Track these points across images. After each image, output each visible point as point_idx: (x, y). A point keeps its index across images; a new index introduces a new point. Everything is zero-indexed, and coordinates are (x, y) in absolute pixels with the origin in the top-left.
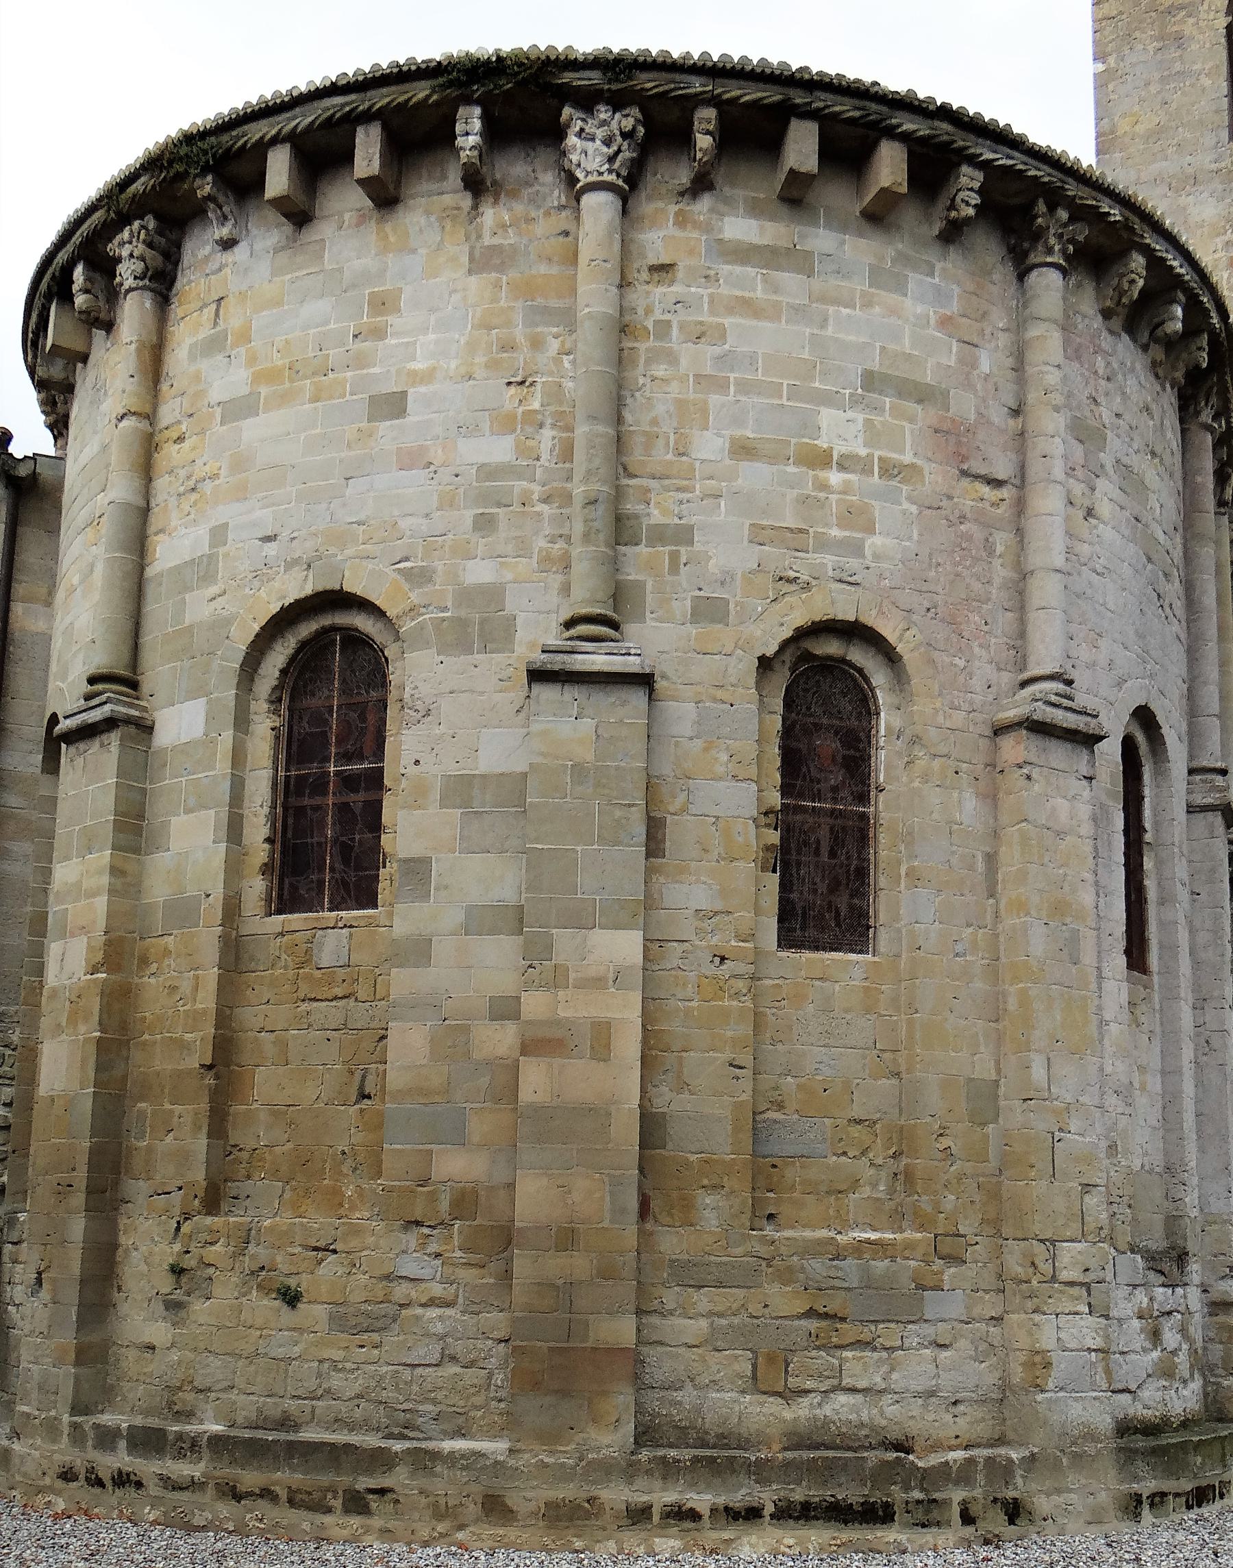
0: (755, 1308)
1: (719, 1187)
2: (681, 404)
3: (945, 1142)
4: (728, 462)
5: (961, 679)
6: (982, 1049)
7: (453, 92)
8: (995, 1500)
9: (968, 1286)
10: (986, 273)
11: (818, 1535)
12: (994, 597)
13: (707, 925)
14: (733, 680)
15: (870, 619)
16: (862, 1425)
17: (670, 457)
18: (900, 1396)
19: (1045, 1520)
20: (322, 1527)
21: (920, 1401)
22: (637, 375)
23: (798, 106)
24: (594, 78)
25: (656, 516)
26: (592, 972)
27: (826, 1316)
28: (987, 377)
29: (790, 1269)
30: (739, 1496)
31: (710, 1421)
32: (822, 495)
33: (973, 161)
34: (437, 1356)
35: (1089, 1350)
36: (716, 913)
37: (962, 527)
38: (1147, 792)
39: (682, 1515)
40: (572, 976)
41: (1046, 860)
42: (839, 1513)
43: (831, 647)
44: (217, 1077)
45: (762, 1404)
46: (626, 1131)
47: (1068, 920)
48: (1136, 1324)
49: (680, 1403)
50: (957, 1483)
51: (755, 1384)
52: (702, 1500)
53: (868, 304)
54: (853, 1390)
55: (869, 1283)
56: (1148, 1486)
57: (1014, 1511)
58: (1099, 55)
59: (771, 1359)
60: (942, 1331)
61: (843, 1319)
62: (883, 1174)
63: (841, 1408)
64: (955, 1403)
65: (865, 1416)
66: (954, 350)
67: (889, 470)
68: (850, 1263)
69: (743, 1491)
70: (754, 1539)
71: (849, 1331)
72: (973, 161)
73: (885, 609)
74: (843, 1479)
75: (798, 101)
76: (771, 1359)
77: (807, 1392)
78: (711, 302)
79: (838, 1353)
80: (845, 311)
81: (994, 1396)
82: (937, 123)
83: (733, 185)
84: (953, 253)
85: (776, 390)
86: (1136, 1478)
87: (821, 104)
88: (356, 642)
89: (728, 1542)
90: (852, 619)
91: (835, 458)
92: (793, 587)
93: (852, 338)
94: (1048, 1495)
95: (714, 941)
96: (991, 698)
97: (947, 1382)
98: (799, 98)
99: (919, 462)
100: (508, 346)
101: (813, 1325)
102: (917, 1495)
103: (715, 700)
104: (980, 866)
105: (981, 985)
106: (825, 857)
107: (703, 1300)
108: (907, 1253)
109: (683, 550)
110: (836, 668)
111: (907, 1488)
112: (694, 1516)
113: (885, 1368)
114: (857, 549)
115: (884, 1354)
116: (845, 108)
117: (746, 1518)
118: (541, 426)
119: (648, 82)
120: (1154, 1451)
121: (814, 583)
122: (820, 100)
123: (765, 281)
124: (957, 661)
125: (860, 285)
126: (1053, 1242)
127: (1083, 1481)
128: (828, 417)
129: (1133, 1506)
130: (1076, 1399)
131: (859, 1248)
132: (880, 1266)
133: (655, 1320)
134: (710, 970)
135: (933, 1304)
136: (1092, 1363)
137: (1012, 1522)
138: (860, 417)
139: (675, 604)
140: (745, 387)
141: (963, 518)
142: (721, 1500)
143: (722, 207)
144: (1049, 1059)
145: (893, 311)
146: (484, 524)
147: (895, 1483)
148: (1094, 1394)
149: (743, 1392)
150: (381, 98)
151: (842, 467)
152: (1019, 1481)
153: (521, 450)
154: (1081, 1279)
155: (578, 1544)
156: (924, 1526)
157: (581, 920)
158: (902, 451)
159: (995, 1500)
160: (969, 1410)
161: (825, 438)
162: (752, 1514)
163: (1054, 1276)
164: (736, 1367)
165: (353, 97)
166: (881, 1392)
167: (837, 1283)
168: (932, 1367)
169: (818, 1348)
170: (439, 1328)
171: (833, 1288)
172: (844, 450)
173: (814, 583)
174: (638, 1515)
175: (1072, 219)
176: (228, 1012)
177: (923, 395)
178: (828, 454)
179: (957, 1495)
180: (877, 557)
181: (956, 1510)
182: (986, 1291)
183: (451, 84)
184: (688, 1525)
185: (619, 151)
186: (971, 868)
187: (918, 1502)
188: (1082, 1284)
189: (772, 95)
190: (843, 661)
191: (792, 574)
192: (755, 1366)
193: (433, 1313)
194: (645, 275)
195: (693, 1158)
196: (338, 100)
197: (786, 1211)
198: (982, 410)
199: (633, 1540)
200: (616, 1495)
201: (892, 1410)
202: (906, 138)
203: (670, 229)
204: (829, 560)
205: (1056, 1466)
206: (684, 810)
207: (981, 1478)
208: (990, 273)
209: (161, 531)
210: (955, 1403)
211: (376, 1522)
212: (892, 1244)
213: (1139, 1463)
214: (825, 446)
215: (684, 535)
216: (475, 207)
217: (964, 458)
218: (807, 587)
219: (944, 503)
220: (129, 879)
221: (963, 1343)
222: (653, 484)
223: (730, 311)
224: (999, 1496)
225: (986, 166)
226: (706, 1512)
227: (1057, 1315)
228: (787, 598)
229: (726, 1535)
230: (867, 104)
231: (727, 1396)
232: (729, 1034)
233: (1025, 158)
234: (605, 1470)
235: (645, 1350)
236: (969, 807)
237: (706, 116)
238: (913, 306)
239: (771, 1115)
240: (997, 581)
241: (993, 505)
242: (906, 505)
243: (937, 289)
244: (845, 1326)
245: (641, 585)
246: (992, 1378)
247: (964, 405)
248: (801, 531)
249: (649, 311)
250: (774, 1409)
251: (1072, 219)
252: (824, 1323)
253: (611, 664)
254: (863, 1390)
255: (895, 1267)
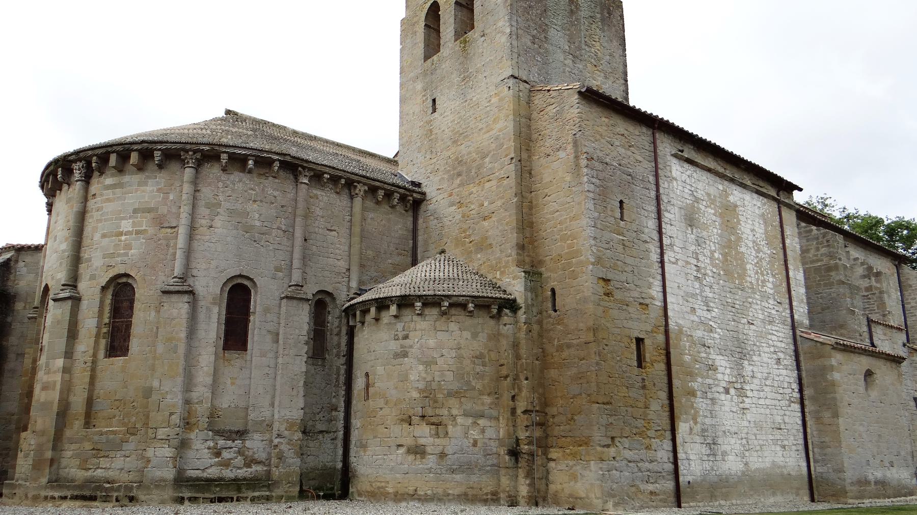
1: (77, 419)
8: (126, 496)
11: (78, 503)
16: (103, 477)
22: (86, 223)
24: (73, 157)
25: (86, 256)
27: (97, 450)
30: (63, 494)
33: (156, 150)
35: (167, 457)
42: (84, 498)
43: (124, 280)
46: (55, 408)
48: (207, 451)
50: (116, 491)
52: (56, 494)
53: (136, 191)
54: (102, 468)
56: (187, 495)
57: (132, 499)
63: (99, 473)
67: (138, 233)
71: (102, 453)
72: (156, 150)
82: (143, 144)
86: (182, 492)
88: (127, 284)
98: (110, 149)
101: (94, 452)
102: (104, 494)
107: (73, 446)
116: (120, 148)
119: (81, 155)
120: (191, 485)
129: (181, 501)
131: (107, 432)
132: (112, 436)
134: (83, 366)
135: (125, 446)
136: (169, 461)
138: (131, 221)
140: (106, 220)
145: (143, 191)
151: (125, 235)
152: (135, 491)
154: (166, 438)
175: (194, 153)
177: (149, 210)
178: (122, 232)
179: (115, 494)
202: (136, 150)
204: (119, 259)
205: (148, 488)
215: (89, 260)
217: (162, 224)
219: (155, 237)
221: (134, 456)
225: (159, 150)
229: (60, 503)
237: (95, 158)
238: (149, 189)
242: (142, 240)
247: (163, 210)
251: (194, 153)
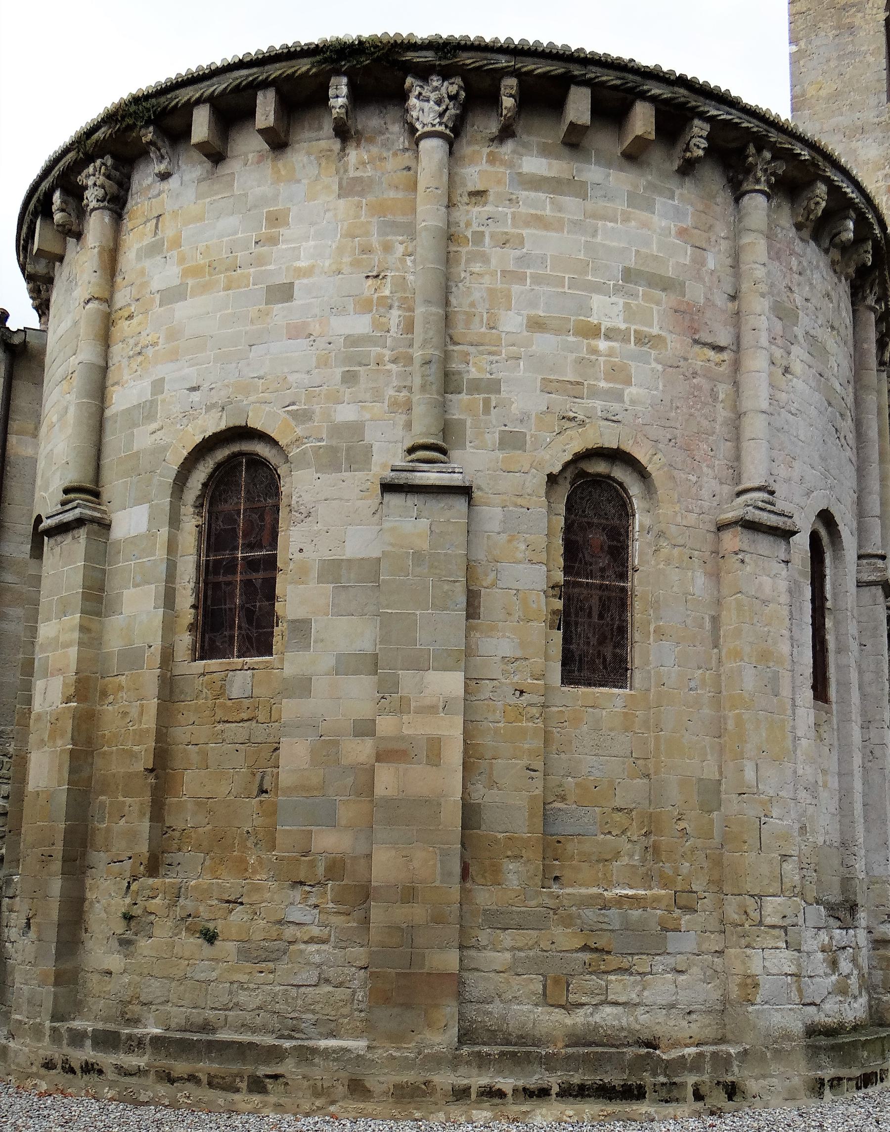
0: (545, 945)
1: (519, 857)
2: (491, 292)
3: (682, 825)
4: (525, 333)
5: (694, 490)
6: (709, 757)
7: (327, 67)
8: (718, 1083)
9: (698, 928)
10: (712, 197)
11: (590, 1108)
12: (717, 431)
13: (510, 668)
14: (529, 491)
15: (628, 447)
16: (622, 1029)
17: (483, 330)
18: (650, 1008)
19: (754, 1097)
20: (233, 1102)
21: (664, 1012)
22: (460, 271)
23: (576, 76)
24: (429, 56)
25: (473, 373)
26: (427, 702)
27: (596, 950)
28: (712, 272)
29: (570, 916)
30: (534, 1080)
31: (512, 1026)
32: (593, 357)
33: (702, 116)
34: (316, 979)
35: (786, 975)
36: (517, 659)
37: (694, 381)
38: (828, 571)
39: (492, 1094)
40: (413, 704)
41: (755, 621)
42: (606, 1092)
43: (600, 467)
44: (157, 778)
45: (550, 1014)
46: (452, 817)
47: (771, 664)
48: (820, 956)
49: (491, 1013)
50: (691, 1070)
51: (545, 999)
52: (506, 1083)
53: (626, 219)
54: (616, 1004)
55: (627, 926)
56: (828, 1073)
57: (732, 1091)
58: (794, 40)
59: (556, 981)
60: (680, 961)
61: (609, 953)
62: (638, 847)
63: (607, 1017)
64: (689, 1013)
65: (624, 1022)
66: (689, 252)
67: (642, 339)
68: (614, 912)
69: (537, 1077)
70: (544, 1111)
71: (613, 961)
72: (702, 116)
73: (639, 440)
74: (608, 1068)
75: (576, 73)
76: (556, 981)
77: (583, 1005)
78: (513, 218)
79: (605, 977)
80: (610, 225)
81: (717, 1008)
82: (676, 89)
83: (529, 133)
84: (688, 183)
85: (560, 282)
86: (820, 1067)
87: (593, 75)
88: (257, 463)
89: (526, 1113)
90: (615, 447)
91: (603, 330)
92: (572, 424)
93: (615, 244)
94: (757, 1079)
95: (516, 679)
96: (715, 504)
97: (683, 998)
98: (577, 71)
99: (664, 334)
100: (367, 250)
101: (587, 956)
102: (662, 1079)
103: (516, 505)
104: (708, 625)
105: (708, 711)
106: (595, 619)
107: (507, 938)
108: (654, 905)
109: (493, 397)
110: (603, 482)
111: (655, 1074)
112: (501, 1094)
113: (639, 988)
114: (619, 397)
115: (638, 978)
116: (610, 78)
117: (539, 1096)
118: (391, 307)
119: (468, 59)
120: (833, 1048)
121: (587, 421)
122: (592, 73)
123: (552, 203)
124: (691, 477)
125: (621, 206)
126: (760, 897)
127: (782, 1069)
128: (597, 301)
129: (818, 1087)
130: (777, 1010)
131: (620, 901)
132: (635, 914)
133: (473, 953)
134: (513, 700)
135: (673, 942)
136: (788, 984)
137: (730, 1099)
138: (621, 301)
139: (487, 436)
140: (538, 280)
141: (695, 374)
142: (521, 1083)
143: (521, 150)
144: (757, 765)
145: (645, 225)
146: (349, 378)
147: (646, 1071)
148: (790, 1006)
149: (536, 1005)
150: (275, 71)
151: (608, 337)
152: (736, 1069)
153: (376, 325)
154: (781, 923)
155: (417, 1115)
156: (667, 1102)
157: (419, 664)
158: (651, 326)
159: (718, 1083)
160: (699, 1018)
161: (595, 316)
162: (543, 1093)
163: (761, 921)
164: (532, 987)
165: (255, 70)
166: (636, 1005)
167: (604, 926)
168: (673, 987)
169: (591, 973)
170: (317, 959)
171: (601, 930)
172: (609, 325)
173: (587, 421)
174: (461, 1094)
175: (774, 158)
176: (165, 731)
177: (666, 285)
178: (597, 327)
179: (691, 1079)
180: (633, 402)
181: (690, 1090)
182: (712, 932)
183: (325, 60)
184: (497, 1101)
185: (447, 109)
186: (701, 626)
187: (663, 1084)
188: (781, 927)
189: (557, 69)
190: (609, 477)
191: (572, 415)
192: (545, 986)
193: (313, 948)
194: (465, 199)
195: (500, 836)
196: (244, 72)
197: (567, 874)
198: (709, 296)
199: (457, 1111)
200: (445, 1079)
201: (644, 1018)
202: (654, 99)
203: (484, 166)
204: (598, 404)
205: (762, 1058)
206: (494, 585)
207: (708, 1067)
208: (714, 197)
209: (117, 383)
210: (689, 1013)
211: (272, 1099)
212: (644, 898)
213: (823, 1056)
214: (596, 322)
215: (494, 386)
216: (343, 149)
217: (696, 331)
218: (582, 424)
219: (682, 363)
220: (93, 635)
221: (695, 970)
222: (471, 349)
223: (527, 224)
224: (721, 1080)
225: (711, 120)
226: (509, 1092)
227: (763, 949)
228: (568, 432)
229: (524, 1108)
230: (626, 75)
231: (525, 1008)
232: (526, 746)
233: (740, 114)
234: (436, 1061)
235: (465, 974)
236: (699, 583)
237: (510, 84)
238: (659, 221)
239: (557, 805)
240: (720, 420)
241: (716, 364)
242: (654, 365)
243: (676, 208)
244: (610, 957)
245: (463, 423)
246: (716, 995)
247: (696, 293)
248: (578, 383)
249: (468, 224)
250: (559, 1017)
251: (774, 158)
252: (595, 955)
253: (441, 479)
254: (623, 1004)
255: (646, 915)
